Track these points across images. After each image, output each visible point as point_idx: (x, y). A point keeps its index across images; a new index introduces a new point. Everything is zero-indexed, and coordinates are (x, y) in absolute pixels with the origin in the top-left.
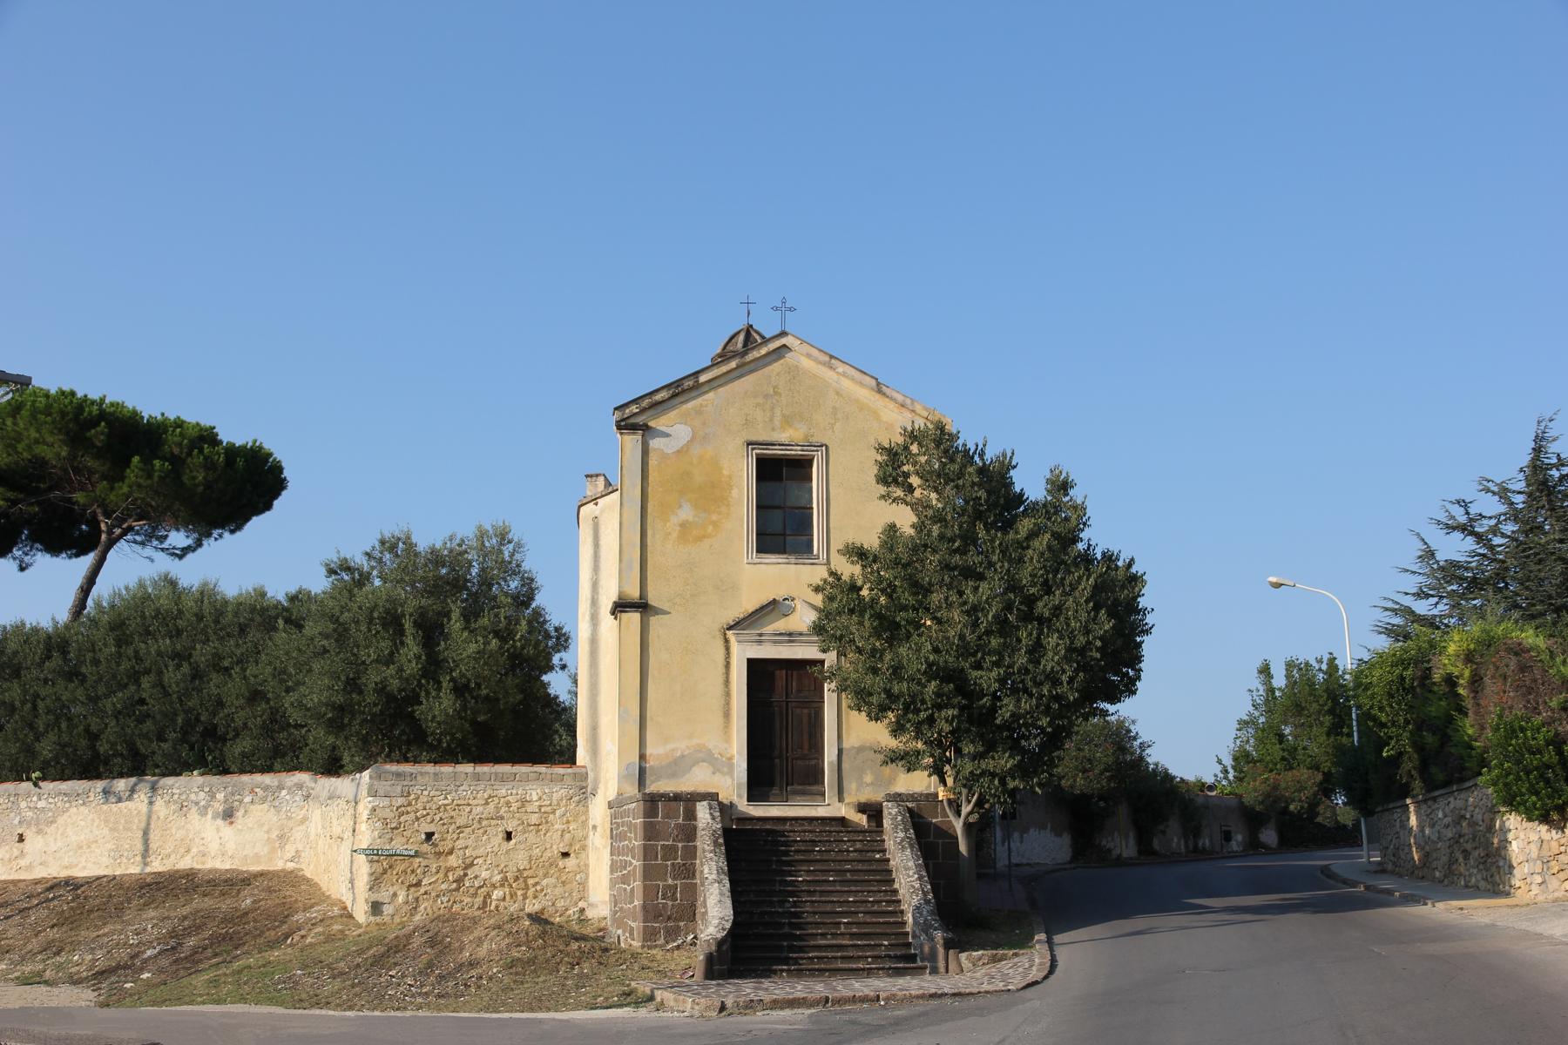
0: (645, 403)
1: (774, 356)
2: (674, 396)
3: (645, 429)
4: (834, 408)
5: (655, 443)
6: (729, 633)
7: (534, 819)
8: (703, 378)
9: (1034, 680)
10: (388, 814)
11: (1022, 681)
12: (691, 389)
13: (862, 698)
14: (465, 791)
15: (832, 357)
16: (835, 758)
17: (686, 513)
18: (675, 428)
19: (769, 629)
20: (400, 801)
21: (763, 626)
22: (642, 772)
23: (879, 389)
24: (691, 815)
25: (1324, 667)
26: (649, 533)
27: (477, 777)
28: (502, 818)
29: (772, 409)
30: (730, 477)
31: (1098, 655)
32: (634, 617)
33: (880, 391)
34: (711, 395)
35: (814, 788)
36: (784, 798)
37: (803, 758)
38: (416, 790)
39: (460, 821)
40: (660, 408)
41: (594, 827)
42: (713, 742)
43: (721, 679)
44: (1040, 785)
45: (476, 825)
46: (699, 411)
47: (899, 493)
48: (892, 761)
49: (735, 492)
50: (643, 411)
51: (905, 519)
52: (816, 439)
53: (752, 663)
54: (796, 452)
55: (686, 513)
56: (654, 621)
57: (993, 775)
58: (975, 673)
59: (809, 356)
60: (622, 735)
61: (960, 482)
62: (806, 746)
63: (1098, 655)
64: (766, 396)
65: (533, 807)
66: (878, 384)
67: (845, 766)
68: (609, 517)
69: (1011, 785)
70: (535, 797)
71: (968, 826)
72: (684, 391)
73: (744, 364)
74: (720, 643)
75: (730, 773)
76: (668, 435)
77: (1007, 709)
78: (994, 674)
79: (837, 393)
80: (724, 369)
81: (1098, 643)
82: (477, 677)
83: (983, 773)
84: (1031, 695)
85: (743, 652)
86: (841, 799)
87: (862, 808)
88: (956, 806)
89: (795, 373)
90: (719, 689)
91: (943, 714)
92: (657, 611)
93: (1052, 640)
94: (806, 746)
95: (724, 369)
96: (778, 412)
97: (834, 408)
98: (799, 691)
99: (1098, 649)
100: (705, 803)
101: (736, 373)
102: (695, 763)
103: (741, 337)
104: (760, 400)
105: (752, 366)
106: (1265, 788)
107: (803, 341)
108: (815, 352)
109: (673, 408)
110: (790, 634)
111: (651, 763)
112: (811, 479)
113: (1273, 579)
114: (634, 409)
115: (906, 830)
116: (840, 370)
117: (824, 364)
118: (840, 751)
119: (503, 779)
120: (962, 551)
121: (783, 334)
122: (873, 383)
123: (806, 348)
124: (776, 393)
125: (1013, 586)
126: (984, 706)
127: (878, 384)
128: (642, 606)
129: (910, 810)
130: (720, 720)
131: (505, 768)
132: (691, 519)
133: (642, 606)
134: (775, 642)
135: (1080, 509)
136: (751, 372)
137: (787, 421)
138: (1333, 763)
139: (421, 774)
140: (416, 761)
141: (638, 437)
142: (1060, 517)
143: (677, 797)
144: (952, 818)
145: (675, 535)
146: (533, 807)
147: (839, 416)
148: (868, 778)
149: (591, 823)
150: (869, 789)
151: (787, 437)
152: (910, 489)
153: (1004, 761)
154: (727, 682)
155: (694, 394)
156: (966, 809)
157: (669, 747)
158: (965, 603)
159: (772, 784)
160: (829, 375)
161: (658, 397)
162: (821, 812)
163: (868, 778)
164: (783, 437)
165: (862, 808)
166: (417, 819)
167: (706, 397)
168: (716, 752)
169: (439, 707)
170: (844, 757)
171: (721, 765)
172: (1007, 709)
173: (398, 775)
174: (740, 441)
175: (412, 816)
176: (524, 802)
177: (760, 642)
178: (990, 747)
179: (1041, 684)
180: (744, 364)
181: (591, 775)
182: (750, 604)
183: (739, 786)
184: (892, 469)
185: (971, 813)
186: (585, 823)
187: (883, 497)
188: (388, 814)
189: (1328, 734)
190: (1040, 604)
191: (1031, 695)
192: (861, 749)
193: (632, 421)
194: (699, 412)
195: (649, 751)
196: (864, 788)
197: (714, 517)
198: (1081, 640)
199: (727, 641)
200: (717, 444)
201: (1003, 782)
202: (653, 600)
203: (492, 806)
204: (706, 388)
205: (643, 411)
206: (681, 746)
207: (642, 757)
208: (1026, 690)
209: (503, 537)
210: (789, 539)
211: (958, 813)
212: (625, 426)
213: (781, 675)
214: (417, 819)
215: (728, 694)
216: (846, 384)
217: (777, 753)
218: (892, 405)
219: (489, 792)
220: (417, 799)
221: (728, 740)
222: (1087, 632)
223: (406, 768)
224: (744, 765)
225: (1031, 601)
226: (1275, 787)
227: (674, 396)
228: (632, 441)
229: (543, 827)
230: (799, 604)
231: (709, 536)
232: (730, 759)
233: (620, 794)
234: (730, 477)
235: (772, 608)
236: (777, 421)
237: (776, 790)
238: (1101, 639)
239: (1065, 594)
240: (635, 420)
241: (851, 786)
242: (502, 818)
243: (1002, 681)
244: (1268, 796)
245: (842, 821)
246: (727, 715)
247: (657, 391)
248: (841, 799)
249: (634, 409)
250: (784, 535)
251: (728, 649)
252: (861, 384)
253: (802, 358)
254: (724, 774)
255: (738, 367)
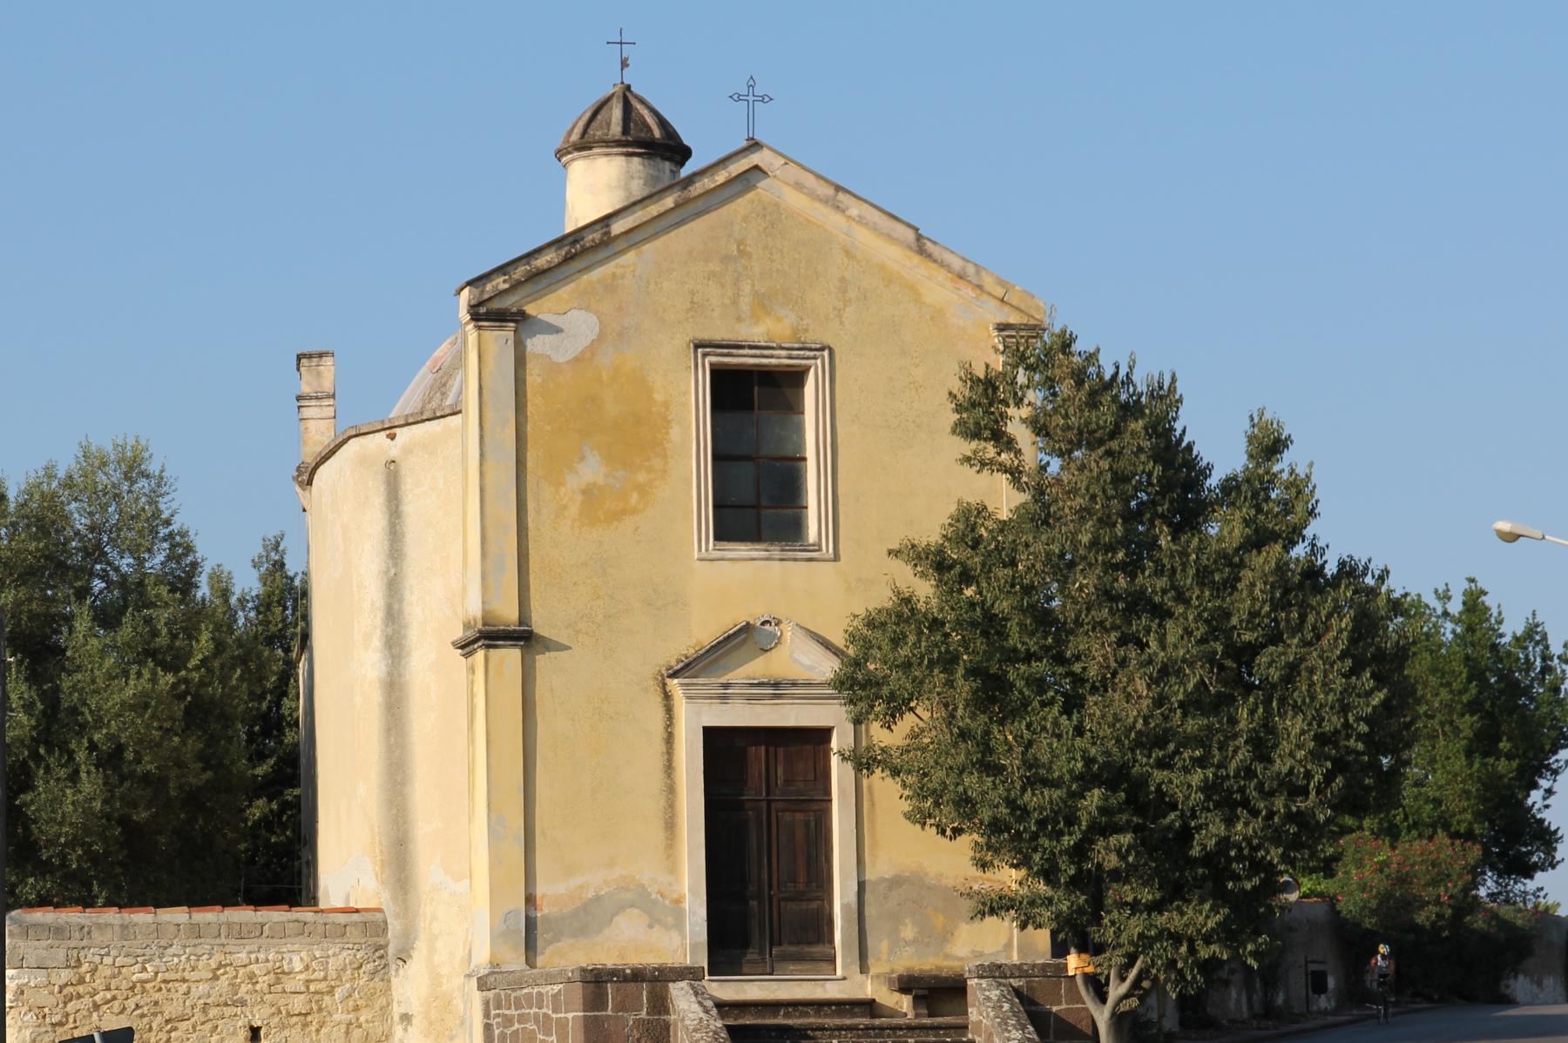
0: (520, 272)
1: (738, 187)
2: (568, 259)
3: (519, 318)
4: (843, 280)
5: (537, 344)
6: (674, 684)
7: (298, 1004)
8: (618, 227)
9: (1260, 787)
10: (45, 998)
11: (1242, 790)
12: (596, 247)
13: (943, 806)
14: (176, 956)
15: (838, 188)
16: (853, 898)
17: (592, 470)
18: (570, 317)
19: (738, 675)
20: (66, 975)
21: (728, 670)
22: (530, 924)
23: (920, 246)
24: (660, 1004)
25: (1455, 607)
26: (531, 505)
27: (197, 932)
28: (243, 1003)
29: (737, 281)
30: (666, 405)
31: (1360, 746)
32: (511, 656)
33: (921, 251)
34: (630, 256)
35: (817, 949)
36: (768, 968)
37: (798, 897)
38: (91, 955)
39: (170, 1010)
40: (544, 281)
41: (406, 1018)
42: (648, 873)
43: (658, 763)
44: (1256, 954)
45: (199, 1017)
46: (611, 287)
47: (990, 451)
48: (993, 911)
49: (675, 433)
50: (516, 286)
51: (1004, 500)
52: (814, 336)
53: (711, 734)
54: (778, 360)
55: (592, 470)
56: (543, 661)
57: (1176, 938)
58: (1159, 775)
59: (799, 186)
60: (495, 862)
61: (1114, 445)
62: (802, 878)
63: (1360, 746)
64: (726, 259)
65: (295, 984)
66: (919, 237)
67: (870, 911)
68: (447, 472)
69: (1204, 953)
70: (298, 966)
71: (1118, 1019)
72: (585, 251)
73: (687, 201)
74: (657, 699)
75: (679, 925)
76: (558, 330)
77: (1211, 831)
78: (1197, 778)
79: (848, 253)
80: (654, 210)
81: (1363, 728)
82: (140, 742)
83: (1159, 937)
84: (1255, 813)
85: (694, 717)
86: (864, 969)
87: (906, 984)
88: (1098, 987)
89: (773, 216)
90: (657, 779)
91: (1113, 840)
92: (548, 645)
93: (1294, 725)
94: (802, 878)
95: (654, 210)
96: (746, 288)
97: (843, 280)
98: (787, 782)
99: (1360, 737)
100: (684, 984)
101: (672, 219)
102: (621, 908)
103: (617, 113)
104: (714, 266)
105: (700, 204)
106: (1378, 883)
107: (789, 160)
108: (810, 181)
109: (566, 279)
110: (776, 685)
111: (544, 911)
112: (801, 412)
113: (1505, 526)
114: (500, 283)
115: (1023, 1028)
116: (854, 212)
117: (825, 201)
118: (861, 886)
119: (240, 934)
120: (1132, 568)
121: (754, 145)
122: (910, 235)
123: (793, 172)
124: (742, 253)
125: (1217, 624)
126: (1170, 827)
127: (919, 237)
128: (523, 637)
129: (1017, 992)
130: (659, 835)
131: (243, 915)
132: (601, 481)
133: (523, 637)
134: (750, 698)
135: (1299, 487)
136: (699, 214)
137: (763, 304)
138: (1479, 816)
139: (100, 927)
140: (87, 903)
141: (507, 334)
142: (1271, 500)
143: (638, 976)
144: (1090, 1004)
145: (574, 510)
146: (295, 984)
147: (852, 295)
148: (908, 932)
149: (397, 1011)
150: (910, 950)
151: (763, 335)
152: (1008, 444)
153: (1200, 916)
154: (669, 768)
155: (601, 255)
156: (1116, 990)
157: (576, 881)
158: (1150, 662)
159: (745, 944)
160: (833, 220)
161: (541, 262)
162: (831, 991)
163: (908, 932)
164: (756, 332)
165: (906, 984)
166: (96, 1007)
167: (622, 260)
168: (653, 890)
169: (68, 801)
170: (868, 896)
171: (661, 912)
172: (1211, 831)
173: (58, 931)
174: (682, 339)
175: (87, 1001)
176: (280, 974)
177: (724, 698)
178: (1174, 893)
179: (1271, 794)
180: (687, 201)
181: (394, 927)
182: (704, 631)
183: (694, 947)
184: (981, 411)
185: (1126, 996)
186: (385, 1010)
187: (967, 460)
188: (45, 998)
189: (1469, 753)
190: (1262, 659)
191: (1255, 813)
192: (896, 882)
193: (497, 305)
194: (611, 287)
195: (541, 890)
196: (903, 952)
197: (641, 477)
198: (1333, 722)
199: (667, 697)
200: (647, 346)
201: (1192, 951)
202: (540, 626)
203: (224, 982)
204: (621, 245)
205: (516, 286)
206: (593, 881)
207: (530, 900)
208: (1245, 803)
209: (133, 467)
210: (765, 512)
211: (1102, 997)
212: (483, 314)
213: (758, 753)
214: (96, 1007)
215: (671, 790)
216: (863, 237)
217: (753, 888)
218: (942, 275)
219: (218, 957)
220: (94, 971)
221: (673, 869)
222: (1345, 709)
223: (72, 916)
224: (702, 912)
225: (1245, 654)
226: (1403, 880)
227: (568, 259)
228: (500, 339)
229: (314, 1019)
230: (788, 631)
231: (634, 511)
232: (678, 901)
233: (494, 964)
234: (666, 405)
235: (744, 639)
236: (745, 304)
237: (752, 955)
238: (1367, 720)
239: (1306, 644)
240: (500, 306)
241: (879, 945)
242: (243, 1003)
243: (1208, 788)
244: (1385, 898)
245: (869, 1007)
246: (670, 825)
247: (538, 251)
248: (864, 969)
249: (500, 283)
250: (757, 507)
251: (669, 710)
252: (889, 237)
253: (782, 190)
254: (667, 928)
255: (677, 206)
